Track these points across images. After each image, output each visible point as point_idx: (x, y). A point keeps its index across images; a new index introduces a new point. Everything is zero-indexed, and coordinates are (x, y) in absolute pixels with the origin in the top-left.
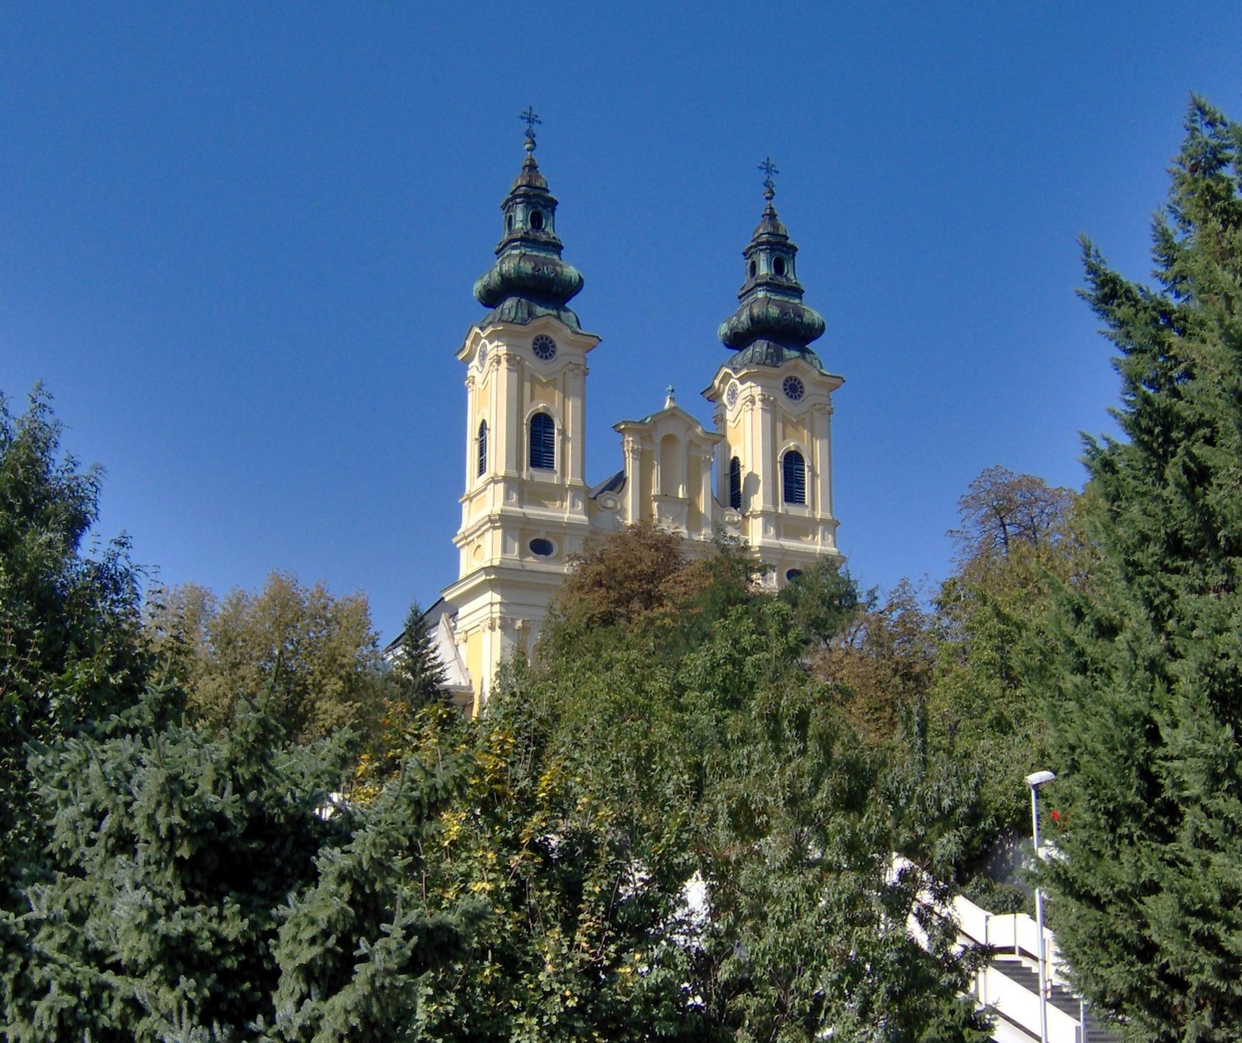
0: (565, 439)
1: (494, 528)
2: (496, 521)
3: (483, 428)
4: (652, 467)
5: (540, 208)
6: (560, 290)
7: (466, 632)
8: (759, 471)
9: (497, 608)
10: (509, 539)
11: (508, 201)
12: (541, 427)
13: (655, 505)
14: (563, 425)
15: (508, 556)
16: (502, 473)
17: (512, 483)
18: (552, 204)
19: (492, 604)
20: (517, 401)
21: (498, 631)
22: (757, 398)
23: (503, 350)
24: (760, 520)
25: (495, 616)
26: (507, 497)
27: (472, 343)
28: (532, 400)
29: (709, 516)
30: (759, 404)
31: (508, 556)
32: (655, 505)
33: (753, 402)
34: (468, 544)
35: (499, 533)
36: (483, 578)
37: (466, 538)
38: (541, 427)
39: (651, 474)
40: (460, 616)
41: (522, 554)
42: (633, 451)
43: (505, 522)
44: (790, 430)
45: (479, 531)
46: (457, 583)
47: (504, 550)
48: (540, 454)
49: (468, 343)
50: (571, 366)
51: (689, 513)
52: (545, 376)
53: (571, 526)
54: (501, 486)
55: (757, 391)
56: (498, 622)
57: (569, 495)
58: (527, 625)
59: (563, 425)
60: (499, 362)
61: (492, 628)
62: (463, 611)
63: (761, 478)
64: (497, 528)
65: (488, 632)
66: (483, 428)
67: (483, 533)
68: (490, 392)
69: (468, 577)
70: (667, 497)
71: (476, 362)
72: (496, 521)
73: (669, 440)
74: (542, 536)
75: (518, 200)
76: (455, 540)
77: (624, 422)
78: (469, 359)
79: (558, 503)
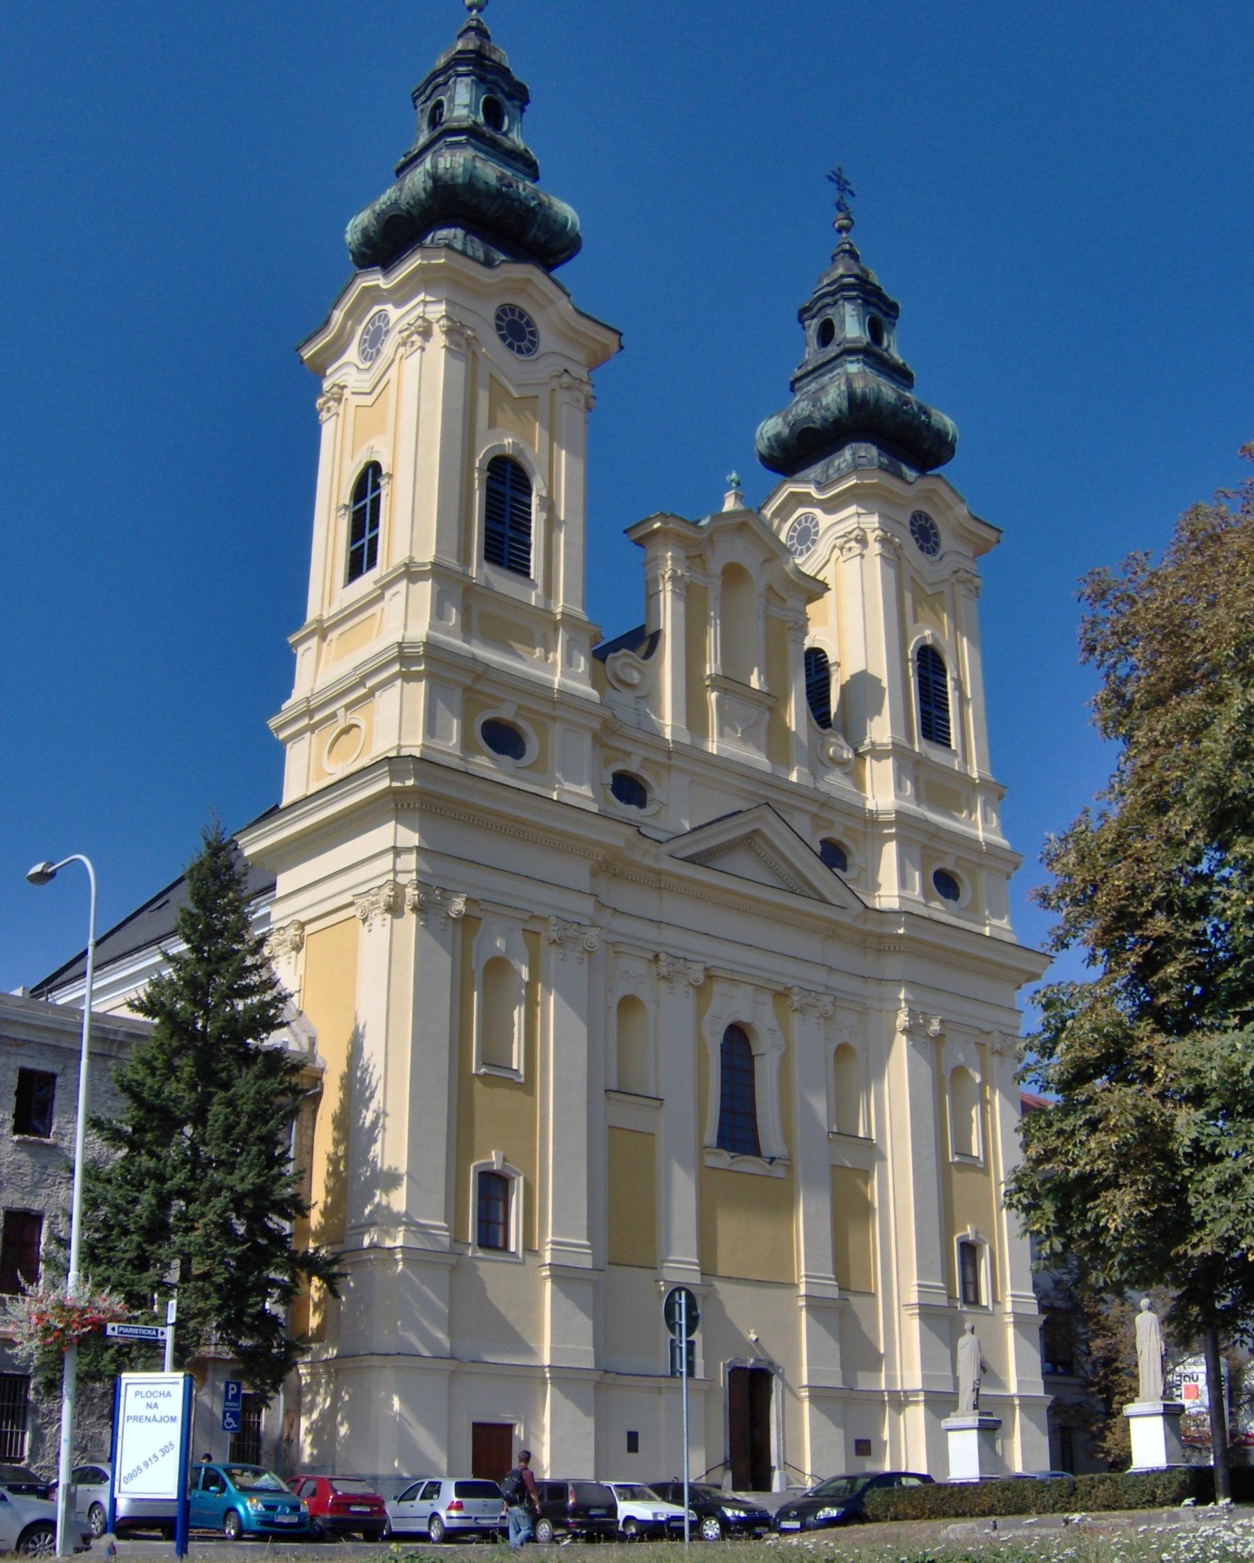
0: (552, 524)
1: (407, 677)
2: (415, 659)
3: (369, 481)
4: (705, 622)
5: (500, 96)
6: (542, 238)
7: (302, 925)
8: (881, 670)
9: (410, 861)
10: (441, 707)
11: (436, 75)
12: (506, 486)
13: (713, 697)
14: (550, 491)
15: (436, 743)
16: (427, 554)
17: (446, 580)
18: (520, 95)
19: (397, 851)
20: (463, 424)
21: (410, 921)
22: (871, 537)
23: (437, 311)
24: (889, 764)
25: (402, 879)
26: (438, 613)
27: (348, 315)
28: (492, 424)
29: (804, 738)
30: (875, 548)
31: (436, 743)
32: (713, 697)
33: (862, 541)
34: (312, 728)
35: (419, 690)
36: (385, 783)
37: (310, 713)
38: (506, 486)
39: (704, 634)
40: (280, 891)
41: (467, 744)
42: (674, 578)
43: (432, 664)
44: (925, 612)
45: (360, 688)
46: (274, 811)
47: (430, 728)
48: (506, 540)
49: (338, 316)
50: (566, 379)
51: (770, 727)
52: (519, 386)
53: (566, 699)
54: (425, 589)
55: (872, 522)
56: (411, 894)
57: (561, 636)
58: (475, 912)
59: (550, 491)
60: (426, 333)
61: (394, 909)
62: (286, 882)
63: (885, 684)
64: (415, 677)
65: (381, 921)
66: (369, 481)
67: (371, 694)
68: (392, 394)
69: (307, 799)
70: (730, 684)
71: (352, 354)
72: (415, 659)
73: (734, 574)
74: (506, 713)
75: (461, 69)
76: (273, 723)
77: (664, 516)
78: (336, 349)
79: (538, 652)
